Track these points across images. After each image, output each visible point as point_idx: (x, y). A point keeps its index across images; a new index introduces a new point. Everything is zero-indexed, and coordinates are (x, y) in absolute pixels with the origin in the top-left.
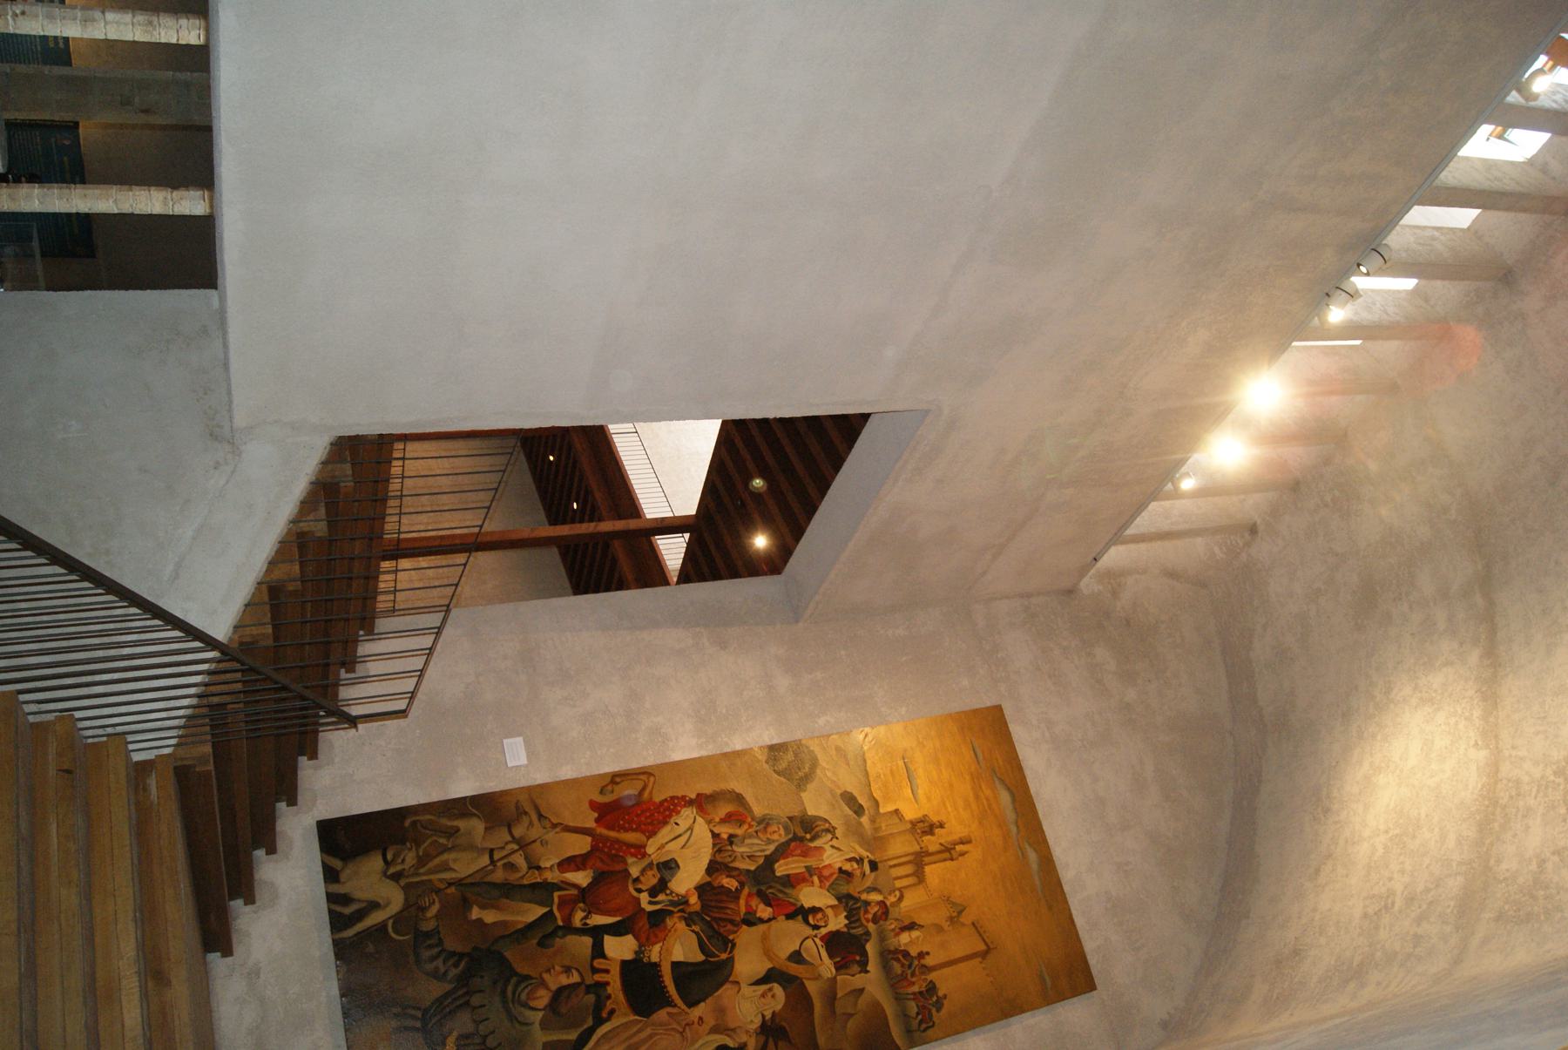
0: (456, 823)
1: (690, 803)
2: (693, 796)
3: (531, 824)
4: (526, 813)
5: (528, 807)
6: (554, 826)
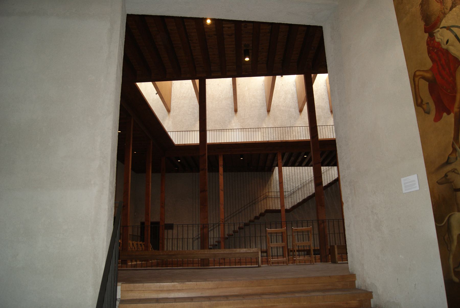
0: (455, 237)
1: (431, 36)
2: (427, 35)
3: (454, 171)
4: (446, 175)
5: (442, 174)
6: (454, 150)
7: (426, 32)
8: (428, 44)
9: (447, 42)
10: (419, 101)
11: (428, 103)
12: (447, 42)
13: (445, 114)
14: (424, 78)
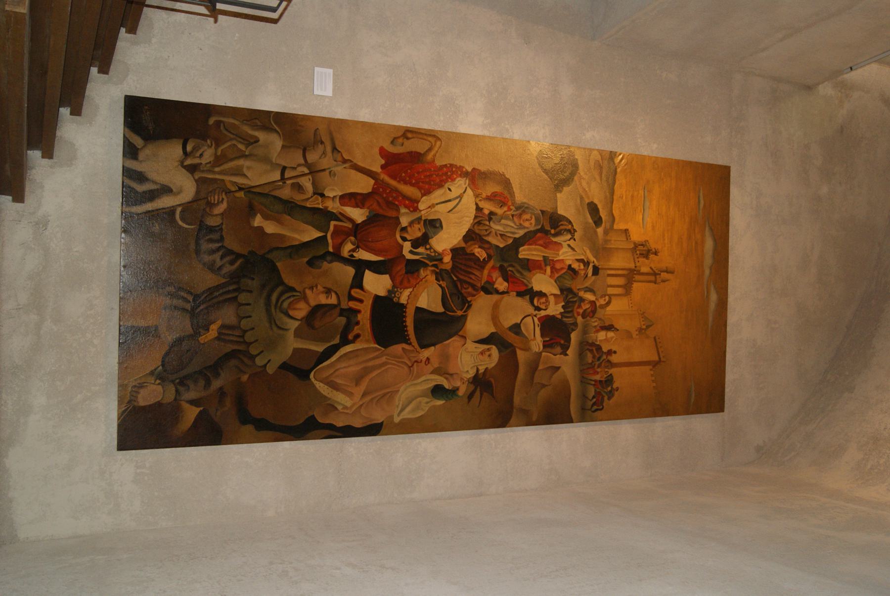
1: (466, 174)
2: (469, 169)
4: (322, 143)
6: (345, 161)
7: (474, 169)
8: (461, 167)
9: (450, 190)
10: (409, 135)
11: (403, 145)
12: (450, 190)
13: (383, 162)
14: (430, 150)
